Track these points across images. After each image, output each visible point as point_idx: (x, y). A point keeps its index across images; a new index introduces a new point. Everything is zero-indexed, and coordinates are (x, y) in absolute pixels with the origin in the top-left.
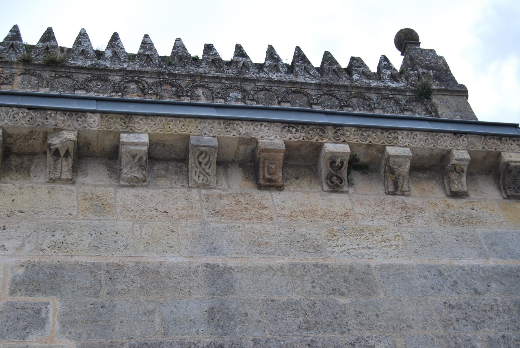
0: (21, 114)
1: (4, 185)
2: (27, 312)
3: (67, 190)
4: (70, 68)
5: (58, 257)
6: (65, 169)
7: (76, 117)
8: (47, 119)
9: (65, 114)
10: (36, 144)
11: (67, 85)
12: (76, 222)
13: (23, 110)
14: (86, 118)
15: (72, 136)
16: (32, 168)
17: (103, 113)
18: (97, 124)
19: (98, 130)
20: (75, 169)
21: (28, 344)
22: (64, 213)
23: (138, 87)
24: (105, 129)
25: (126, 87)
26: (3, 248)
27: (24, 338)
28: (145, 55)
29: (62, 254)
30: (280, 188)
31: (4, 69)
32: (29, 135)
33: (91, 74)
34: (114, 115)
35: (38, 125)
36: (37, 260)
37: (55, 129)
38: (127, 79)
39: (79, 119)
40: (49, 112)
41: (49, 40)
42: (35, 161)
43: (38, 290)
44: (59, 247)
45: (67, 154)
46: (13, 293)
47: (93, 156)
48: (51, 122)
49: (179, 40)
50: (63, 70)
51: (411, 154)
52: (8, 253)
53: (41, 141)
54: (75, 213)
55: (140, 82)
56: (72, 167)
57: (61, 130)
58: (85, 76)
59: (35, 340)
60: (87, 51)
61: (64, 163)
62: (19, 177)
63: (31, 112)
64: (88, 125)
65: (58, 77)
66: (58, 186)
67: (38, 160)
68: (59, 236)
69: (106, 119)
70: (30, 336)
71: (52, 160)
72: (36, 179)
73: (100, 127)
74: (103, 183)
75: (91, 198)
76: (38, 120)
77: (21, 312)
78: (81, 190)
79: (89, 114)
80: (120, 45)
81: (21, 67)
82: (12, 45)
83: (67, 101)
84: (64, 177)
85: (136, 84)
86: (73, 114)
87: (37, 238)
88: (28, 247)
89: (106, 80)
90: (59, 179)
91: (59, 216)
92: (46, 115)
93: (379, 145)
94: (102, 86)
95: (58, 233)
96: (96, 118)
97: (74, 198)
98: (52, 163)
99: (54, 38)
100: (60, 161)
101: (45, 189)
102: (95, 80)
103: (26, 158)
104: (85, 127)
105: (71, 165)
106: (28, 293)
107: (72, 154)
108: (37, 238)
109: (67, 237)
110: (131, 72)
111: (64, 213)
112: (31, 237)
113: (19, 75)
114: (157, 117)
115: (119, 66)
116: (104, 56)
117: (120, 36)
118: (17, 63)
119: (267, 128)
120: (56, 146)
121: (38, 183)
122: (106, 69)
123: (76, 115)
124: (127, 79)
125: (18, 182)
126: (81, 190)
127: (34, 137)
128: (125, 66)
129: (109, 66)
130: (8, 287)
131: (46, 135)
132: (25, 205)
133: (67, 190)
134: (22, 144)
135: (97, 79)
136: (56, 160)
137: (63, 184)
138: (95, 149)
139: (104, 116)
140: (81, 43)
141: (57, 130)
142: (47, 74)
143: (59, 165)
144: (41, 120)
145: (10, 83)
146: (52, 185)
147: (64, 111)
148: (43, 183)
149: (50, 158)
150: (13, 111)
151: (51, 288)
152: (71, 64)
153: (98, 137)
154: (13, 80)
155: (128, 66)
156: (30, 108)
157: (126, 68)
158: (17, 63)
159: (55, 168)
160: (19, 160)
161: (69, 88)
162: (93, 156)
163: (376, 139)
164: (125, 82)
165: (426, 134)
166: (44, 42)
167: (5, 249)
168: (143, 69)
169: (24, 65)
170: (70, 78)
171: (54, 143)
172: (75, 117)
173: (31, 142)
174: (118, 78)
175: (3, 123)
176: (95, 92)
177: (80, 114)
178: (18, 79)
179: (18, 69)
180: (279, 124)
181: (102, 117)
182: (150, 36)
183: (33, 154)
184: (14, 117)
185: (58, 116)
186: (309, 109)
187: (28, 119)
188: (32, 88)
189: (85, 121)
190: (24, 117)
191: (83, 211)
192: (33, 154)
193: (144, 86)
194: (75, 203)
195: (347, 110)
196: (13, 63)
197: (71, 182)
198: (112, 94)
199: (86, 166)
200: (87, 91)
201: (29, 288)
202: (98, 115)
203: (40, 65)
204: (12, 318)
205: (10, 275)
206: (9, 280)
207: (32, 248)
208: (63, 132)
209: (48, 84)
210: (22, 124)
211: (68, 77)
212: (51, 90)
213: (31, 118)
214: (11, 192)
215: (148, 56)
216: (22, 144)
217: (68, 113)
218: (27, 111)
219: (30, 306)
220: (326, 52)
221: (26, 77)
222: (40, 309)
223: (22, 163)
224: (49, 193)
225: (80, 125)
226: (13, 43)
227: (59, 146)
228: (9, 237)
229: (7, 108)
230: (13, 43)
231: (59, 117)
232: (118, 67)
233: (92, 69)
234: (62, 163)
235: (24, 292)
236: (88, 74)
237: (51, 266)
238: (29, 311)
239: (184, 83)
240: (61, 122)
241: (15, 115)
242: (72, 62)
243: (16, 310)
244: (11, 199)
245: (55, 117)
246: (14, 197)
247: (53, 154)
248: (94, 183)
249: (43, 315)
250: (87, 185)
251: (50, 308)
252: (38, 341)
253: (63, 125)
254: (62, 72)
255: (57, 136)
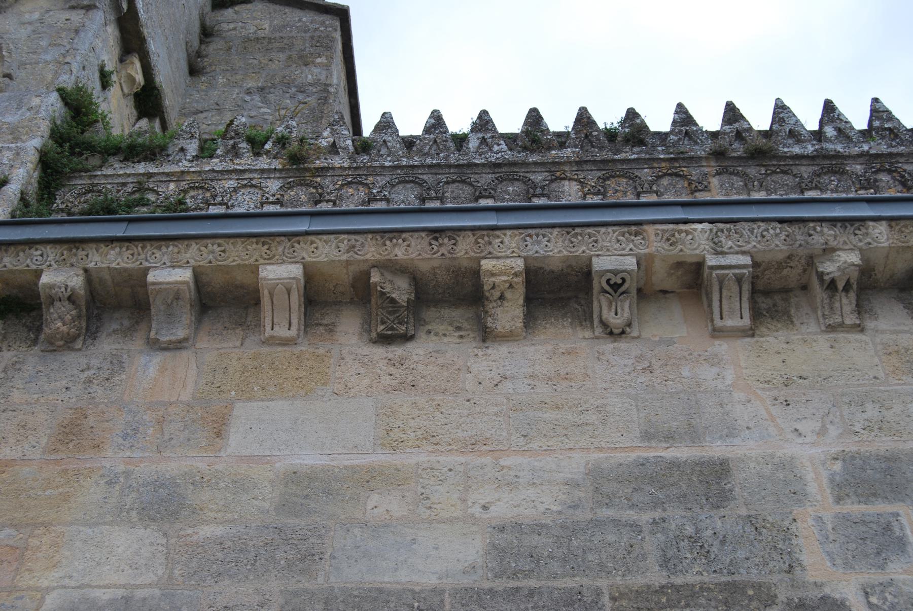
0: (771, 231)
1: (762, 339)
2: (871, 528)
3: (857, 340)
4: (785, 157)
5: (884, 444)
6: (847, 309)
7: (853, 229)
8: (810, 235)
9: (835, 226)
10: (792, 275)
11: (787, 185)
12: (888, 388)
13: (773, 224)
14: (867, 229)
15: (854, 258)
16: (793, 311)
17: (890, 219)
18: (885, 237)
19: (890, 247)
20: (860, 309)
21: (893, 577)
22: (867, 377)
23: (894, 178)
24: (900, 244)
25: (876, 181)
26: (796, 433)
27: (882, 567)
28: (886, 129)
29: (889, 438)
30: (407, 338)
31: (691, 169)
32: (785, 262)
33: (818, 165)
34: (908, 222)
35: (800, 245)
36: (854, 449)
37: (824, 250)
38: (873, 167)
39: (857, 232)
40: (812, 225)
41: (736, 121)
42: (793, 300)
43: (874, 495)
44: (880, 429)
45: (847, 288)
46: (839, 500)
47: (875, 287)
48: (818, 240)
49: (876, 100)
50: (775, 163)
51: (860, 262)
52: (808, 440)
53: (799, 270)
54: (883, 375)
55: (894, 171)
56: (857, 306)
57: (834, 250)
58: (811, 169)
59: (900, 570)
60: (798, 131)
61: (845, 301)
62: (779, 325)
63: (785, 226)
64: (873, 239)
65: (770, 174)
66: (841, 336)
67: (796, 299)
68: (872, 411)
69: (897, 228)
70: (890, 565)
71: (825, 297)
72: (804, 327)
73: (891, 241)
74: (906, 328)
75: (897, 352)
76: (798, 237)
77: (864, 529)
78: (878, 340)
79: (871, 223)
80: (841, 117)
81: (713, 163)
82: (687, 133)
83: (454, 215)
84: (848, 322)
85: (889, 174)
86: (847, 224)
87: (842, 416)
88: (833, 431)
89: (843, 173)
90: (842, 325)
91: (861, 382)
92: (809, 229)
93: (133, 269)
94: (839, 181)
95: (869, 406)
96: (883, 227)
97: (872, 353)
98: (825, 301)
99: (742, 117)
100: (837, 298)
101: (823, 342)
102: (825, 174)
103: (777, 298)
104: (870, 244)
105: (854, 302)
106: (862, 499)
107: (855, 286)
108: (842, 416)
109: (885, 413)
110: (877, 156)
111: (867, 377)
112: (831, 415)
113: (714, 176)
114: (136, 243)
115: (857, 149)
116: (825, 136)
117: (837, 103)
118: (707, 158)
119: (266, 247)
120: (831, 276)
121: (810, 333)
122: (837, 156)
123: (852, 225)
124: (873, 167)
125: (780, 333)
126: (878, 340)
127: (792, 264)
128: (866, 147)
129: (841, 150)
130: (829, 491)
131: (811, 261)
132: (804, 367)
133: (857, 340)
134: (772, 276)
135: (828, 172)
136: (831, 297)
137: (848, 332)
138: (879, 276)
139: (893, 223)
140: (784, 121)
141: (828, 251)
142: (753, 171)
143: (837, 305)
144: (802, 238)
145: (706, 189)
146: (831, 335)
147: (833, 221)
148: (816, 333)
149: (819, 293)
150: (759, 227)
151: (892, 491)
152: (785, 153)
153: (887, 257)
154: (709, 183)
155: (870, 148)
156: (782, 221)
157: (868, 152)
158: (707, 158)
159: (832, 308)
160: (769, 302)
161: (792, 189)
162: (875, 287)
163: (464, 248)
164: (873, 172)
165: (59, 249)
166: (730, 124)
167: (800, 434)
168: (894, 150)
169: (717, 160)
170: (788, 174)
171: (828, 271)
172: (850, 229)
173: (785, 272)
174: (858, 167)
175: (750, 246)
176: (832, 191)
177: (857, 225)
178: (715, 181)
179: (710, 168)
180: (423, 234)
181: (891, 226)
182: (881, 99)
183: (786, 291)
184: (763, 237)
185: (825, 230)
186: (801, 197)
187: (784, 237)
188: (738, 193)
189: (867, 234)
190: (777, 235)
191: (893, 372)
192: (786, 291)
193: (903, 177)
194: (876, 360)
195: (483, 202)
196: (700, 158)
197: (860, 328)
198: (859, 192)
199: (870, 303)
200: (821, 190)
201: (860, 491)
202: (884, 223)
203: (739, 158)
204: (853, 537)
205: (825, 474)
206: (825, 482)
207: (840, 431)
208: (838, 253)
209: (761, 186)
210: (777, 246)
211: (785, 172)
212: (768, 195)
213: (787, 236)
214: (776, 349)
215: (890, 129)
216: (772, 276)
217: (839, 224)
218: (779, 226)
219: (872, 519)
220: (384, 114)
221: (725, 178)
222: (889, 523)
223: (775, 305)
224: (832, 347)
225: (860, 241)
226: (686, 130)
227: (837, 274)
228: (799, 417)
229: (749, 224)
230: (686, 130)
231: (828, 231)
232: (856, 150)
233: (818, 157)
234: (841, 300)
235: (854, 498)
236: (813, 165)
237: (878, 458)
238: (874, 526)
239: (538, 178)
240: (831, 239)
241: (765, 233)
242: (786, 150)
243: (854, 525)
244: (781, 360)
245: (822, 231)
246: (783, 357)
247: (827, 288)
248: (892, 328)
249: (898, 532)
250: (883, 332)
251: (904, 520)
252: (905, 572)
253: (835, 243)
254: (774, 165)
255: (829, 260)
